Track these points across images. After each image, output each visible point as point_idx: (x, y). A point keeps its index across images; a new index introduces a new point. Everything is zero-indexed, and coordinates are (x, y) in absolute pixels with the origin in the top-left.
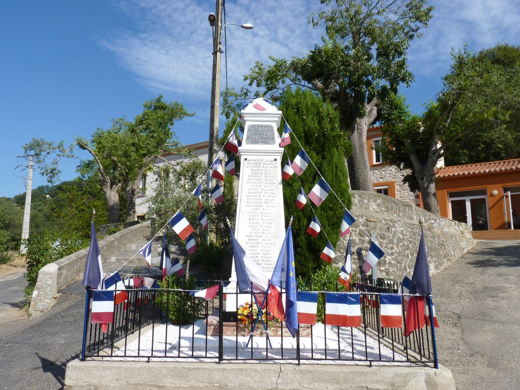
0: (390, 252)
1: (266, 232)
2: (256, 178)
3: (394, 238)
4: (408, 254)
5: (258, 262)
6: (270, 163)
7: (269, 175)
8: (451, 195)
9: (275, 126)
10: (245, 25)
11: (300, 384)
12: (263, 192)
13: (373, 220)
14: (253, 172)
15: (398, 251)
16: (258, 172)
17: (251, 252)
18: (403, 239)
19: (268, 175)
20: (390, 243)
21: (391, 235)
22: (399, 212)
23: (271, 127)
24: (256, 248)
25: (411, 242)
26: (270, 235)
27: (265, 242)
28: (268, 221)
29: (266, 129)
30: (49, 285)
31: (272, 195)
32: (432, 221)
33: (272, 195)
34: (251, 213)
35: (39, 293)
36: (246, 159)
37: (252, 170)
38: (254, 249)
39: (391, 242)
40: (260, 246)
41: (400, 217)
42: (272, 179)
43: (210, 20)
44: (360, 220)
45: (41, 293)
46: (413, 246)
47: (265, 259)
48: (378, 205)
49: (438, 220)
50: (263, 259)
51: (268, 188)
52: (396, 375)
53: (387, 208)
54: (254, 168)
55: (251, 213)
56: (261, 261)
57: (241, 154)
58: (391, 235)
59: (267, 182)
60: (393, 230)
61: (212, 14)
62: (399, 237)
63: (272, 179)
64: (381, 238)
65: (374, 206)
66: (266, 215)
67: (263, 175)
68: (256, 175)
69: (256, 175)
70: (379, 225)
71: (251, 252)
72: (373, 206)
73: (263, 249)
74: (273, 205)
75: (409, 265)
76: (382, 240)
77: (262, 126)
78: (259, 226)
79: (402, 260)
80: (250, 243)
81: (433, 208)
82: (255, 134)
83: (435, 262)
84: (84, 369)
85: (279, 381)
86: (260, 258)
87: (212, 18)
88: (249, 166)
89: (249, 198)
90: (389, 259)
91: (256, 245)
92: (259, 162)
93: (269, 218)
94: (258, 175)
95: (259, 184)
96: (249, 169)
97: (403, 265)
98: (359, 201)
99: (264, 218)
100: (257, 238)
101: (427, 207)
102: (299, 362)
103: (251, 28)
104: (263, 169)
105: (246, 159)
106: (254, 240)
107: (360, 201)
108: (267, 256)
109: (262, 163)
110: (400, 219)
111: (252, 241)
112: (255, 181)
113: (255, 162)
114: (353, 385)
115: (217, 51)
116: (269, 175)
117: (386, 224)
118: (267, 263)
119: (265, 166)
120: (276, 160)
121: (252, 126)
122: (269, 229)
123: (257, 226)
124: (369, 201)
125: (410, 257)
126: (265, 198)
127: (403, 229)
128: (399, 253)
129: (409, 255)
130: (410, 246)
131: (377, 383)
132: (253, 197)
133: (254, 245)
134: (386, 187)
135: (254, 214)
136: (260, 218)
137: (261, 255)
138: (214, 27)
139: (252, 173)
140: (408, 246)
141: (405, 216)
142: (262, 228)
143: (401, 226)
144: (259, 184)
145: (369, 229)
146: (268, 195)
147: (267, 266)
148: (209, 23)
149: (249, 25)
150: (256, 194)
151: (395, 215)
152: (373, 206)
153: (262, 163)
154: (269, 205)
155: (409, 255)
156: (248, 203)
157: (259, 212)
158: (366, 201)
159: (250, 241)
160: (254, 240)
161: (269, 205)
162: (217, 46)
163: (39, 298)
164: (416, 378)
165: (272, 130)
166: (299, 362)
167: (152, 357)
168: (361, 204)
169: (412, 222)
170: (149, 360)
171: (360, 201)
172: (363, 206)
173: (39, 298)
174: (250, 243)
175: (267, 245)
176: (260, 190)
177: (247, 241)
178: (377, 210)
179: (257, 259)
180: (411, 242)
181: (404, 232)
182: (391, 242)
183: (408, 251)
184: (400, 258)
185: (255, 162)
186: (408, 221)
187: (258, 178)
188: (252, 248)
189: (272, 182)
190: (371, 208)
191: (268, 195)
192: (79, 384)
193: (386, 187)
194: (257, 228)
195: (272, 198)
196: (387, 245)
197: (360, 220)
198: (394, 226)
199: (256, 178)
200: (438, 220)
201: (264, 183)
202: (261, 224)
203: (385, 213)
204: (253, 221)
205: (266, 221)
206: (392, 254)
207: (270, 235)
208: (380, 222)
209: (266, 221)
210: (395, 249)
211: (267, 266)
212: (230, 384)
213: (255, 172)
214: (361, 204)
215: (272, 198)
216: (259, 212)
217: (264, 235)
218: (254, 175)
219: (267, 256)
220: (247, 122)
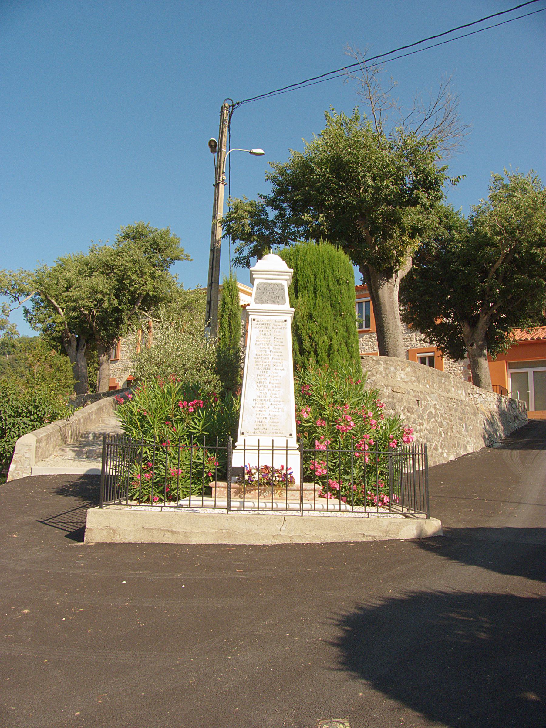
0: (418, 428)
1: (274, 396)
2: (264, 339)
3: (424, 413)
4: (440, 432)
5: (265, 427)
6: (280, 324)
7: (279, 337)
8: (511, 366)
9: (286, 285)
10: (254, 151)
11: (302, 531)
12: (272, 354)
13: (400, 391)
14: (262, 333)
15: (428, 428)
16: (267, 333)
17: (258, 417)
18: (436, 413)
19: (277, 337)
20: (419, 418)
21: (421, 409)
22: (433, 382)
23: (282, 286)
24: (263, 413)
25: (445, 419)
26: (279, 399)
27: (273, 406)
28: (276, 385)
29: (277, 287)
30: (28, 458)
31: (280, 357)
32: (476, 396)
33: (280, 357)
34: (258, 377)
35: (16, 467)
36: (254, 320)
37: (260, 331)
38: (261, 413)
39: (421, 417)
40: (268, 410)
41: (434, 388)
42: (282, 340)
43: (211, 146)
44: (385, 390)
45: (19, 467)
46: (447, 423)
47: (273, 424)
48: (407, 374)
49: (483, 395)
50: (270, 423)
51: (277, 350)
52: (390, 523)
53: (417, 377)
54: (263, 330)
55: (258, 377)
56: (268, 426)
57: (250, 313)
58: (421, 409)
59: (276, 344)
60: (423, 403)
61: (213, 139)
62: (431, 412)
63: (282, 340)
64: (409, 412)
65: (402, 375)
66: (275, 378)
67: (272, 337)
68: (264, 336)
69: (264, 336)
70: (406, 397)
71: (258, 417)
72: (401, 375)
73: (271, 413)
74: (282, 368)
75: (441, 445)
76: (409, 415)
77: (272, 284)
78: (266, 390)
79: (432, 439)
80: (257, 407)
81: (483, 381)
82: (265, 293)
83: (474, 443)
84: (104, 514)
85: (283, 528)
86: (267, 423)
87: (213, 144)
88: (258, 326)
89: (257, 360)
90: (417, 437)
91: (263, 409)
92: (268, 322)
93: (277, 382)
94: (267, 336)
95: (268, 346)
96: (258, 330)
97: (434, 444)
98: (385, 369)
99: (272, 382)
100: (264, 402)
101: (476, 381)
102: (302, 514)
103: (263, 154)
104: (273, 330)
105: (254, 320)
106: (261, 404)
107: (387, 369)
108: (275, 420)
109: (271, 324)
110: (434, 391)
111: (259, 406)
112: (264, 343)
113: (264, 323)
114: (350, 533)
115: (219, 183)
116: (279, 337)
117: (415, 396)
118: (274, 428)
119: (274, 327)
120: (285, 321)
121: (261, 284)
122: (277, 393)
123: (264, 390)
124: (396, 369)
125: (443, 436)
126: (273, 360)
127: (436, 402)
128: (429, 431)
129: (442, 433)
130: (444, 423)
131: (372, 531)
132: (261, 359)
133: (261, 409)
134: (432, 354)
135: (262, 377)
136: (268, 381)
137: (269, 419)
138: (216, 154)
139: (260, 334)
140: (441, 422)
141: (440, 387)
142: (270, 392)
143: (434, 399)
144: (268, 346)
145: (395, 401)
146: (277, 357)
147: (274, 431)
148: (209, 149)
149: (260, 151)
150: (265, 357)
151: (428, 386)
152: (401, 375)
153: (271, 324)
154: (277, 368)
155: (442, 433)
156: (256, 365)
157: (267, 375)
158: (392, 369)
159: (257, 405)
160: (261, 404)
161: (277, 368)
162: (220, 176)
163: (17, 472)
164: (408, 526)
165: (283, 289)
166: (302, 514)
167: (162, 507)
168: (387, 372)
169: (449, 395)
170: (161, 509)
171: (387, 369)
172: (389, 375)
173: (17, 472)
174: (257, 407)
175: (274, 410)
176: (268, 352)
177: (254, 405)
178: (406, 380)
179: (264, 424)
180: (445, 419)
181: (438, 407)
182: (421, 417)
183: (441, 429)
184: (430, 436)
185: (264, 323)
186: (446, 394)
187: (267, 340)
188: (259, 412)
189: (281, 344)
190: (399, 377)
191: (277, 357)
192: (99, 527)
193: (432, 354)
194: (265, 392)
195: (281, 361)
196: (415, 420)
197: (385, 390)
198: (425, 399)
199: (264, 339)
200: (483, 395)
201: (273, 345)
202: (269, 387)
203: (415, 384)
204: (261, 384)
205: (274, 385)
206: (421, 431)
207: (279, 399)
208: (409, 393)
209: (274, 385)
210: (425, 426)
211: (274, 431)
212: (238, 531)
213: (263, 333)
214: (387, 372)
215: (281, 361)
216: (267, 375)
217: (272, 399)
218: (262, 336)
219: (275, 420)
220: (256, 280)
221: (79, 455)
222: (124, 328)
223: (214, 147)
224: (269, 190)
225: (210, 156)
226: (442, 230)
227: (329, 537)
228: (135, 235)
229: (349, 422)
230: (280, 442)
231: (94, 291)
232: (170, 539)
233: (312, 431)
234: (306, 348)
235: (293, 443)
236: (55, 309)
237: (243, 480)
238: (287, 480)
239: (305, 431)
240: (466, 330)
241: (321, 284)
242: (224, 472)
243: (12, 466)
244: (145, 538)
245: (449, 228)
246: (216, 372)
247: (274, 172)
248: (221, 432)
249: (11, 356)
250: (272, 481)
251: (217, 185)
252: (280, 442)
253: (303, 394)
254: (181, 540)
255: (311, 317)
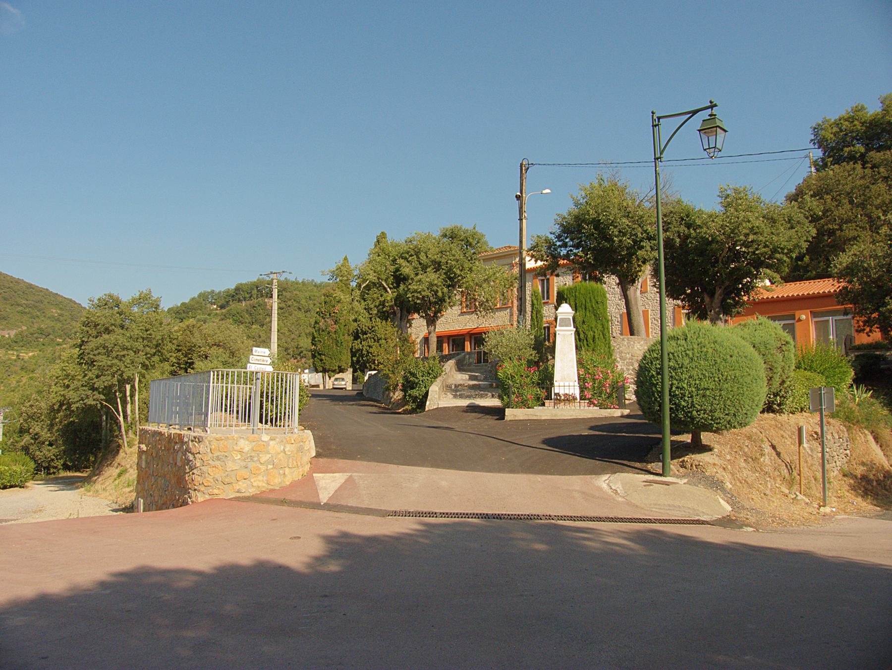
10: (544, 192)
221: (455, 396)
222: (446, 304)
223: (518, 198)
224: (557, 229)
225: (517, 203)
226: (683, 228)
227: (590, 416)
228: (452, 235)
229: (271, 439)
230: (572, 384)
231: (431, 285)
232: (535, 418)
233: (584, 379)
234: (581, 341)
235: (576, 384)
236: (385, 289)
237: (558, 400)
238: (574, 399)
239: (581, 379)
240: (707, 299)
241: (589, 305)
242: (549, 397)
243: (428, 403)
244: (527, 418)
245: (689, 226)
246: (534, 349)
247: (559, 220)
248: (546, 380)
249: (248, 302)
250: (569, 399)
251: (521, 220)
252: (572, 384)
253: (580, 363)
254: (539, 418)
255: (584, 322)
